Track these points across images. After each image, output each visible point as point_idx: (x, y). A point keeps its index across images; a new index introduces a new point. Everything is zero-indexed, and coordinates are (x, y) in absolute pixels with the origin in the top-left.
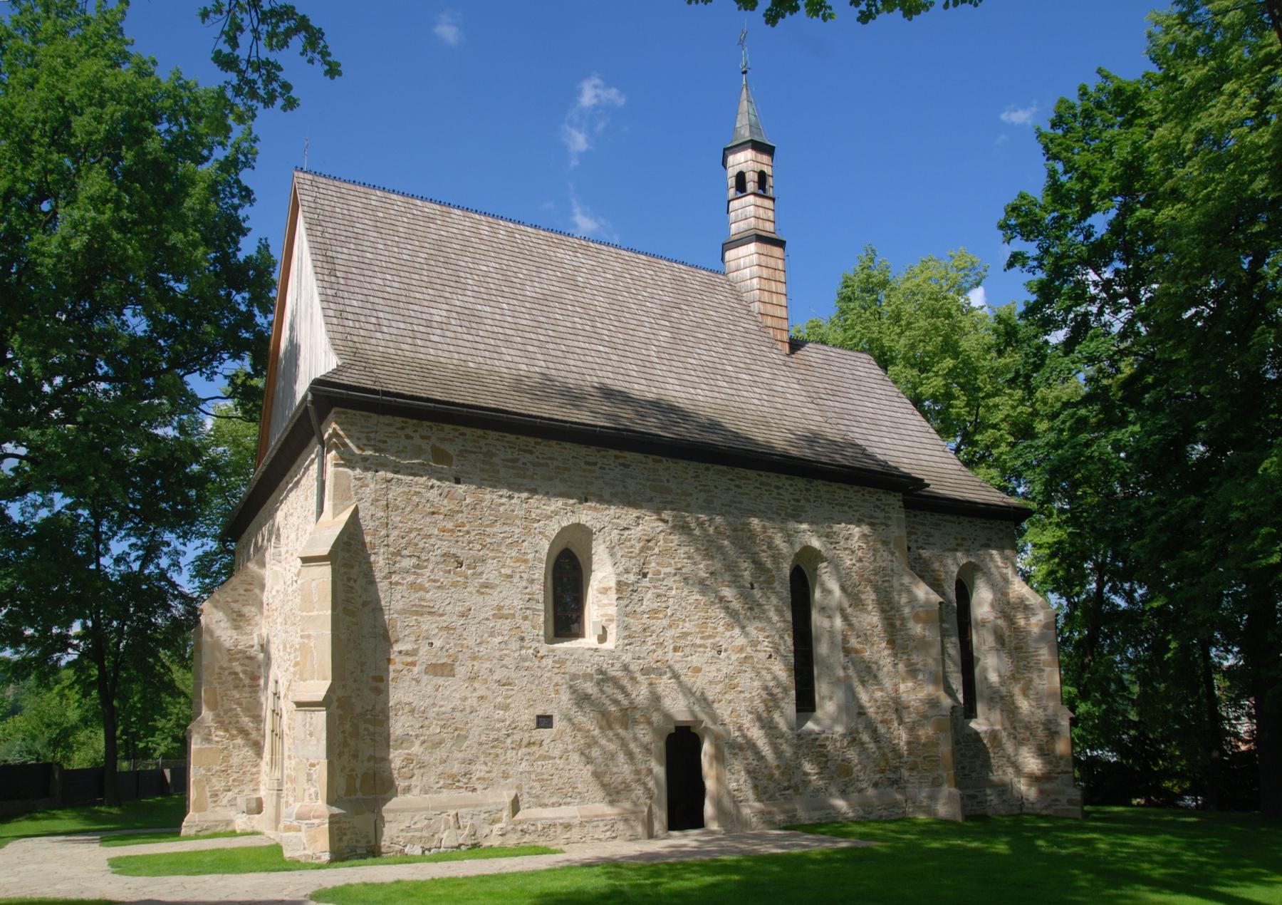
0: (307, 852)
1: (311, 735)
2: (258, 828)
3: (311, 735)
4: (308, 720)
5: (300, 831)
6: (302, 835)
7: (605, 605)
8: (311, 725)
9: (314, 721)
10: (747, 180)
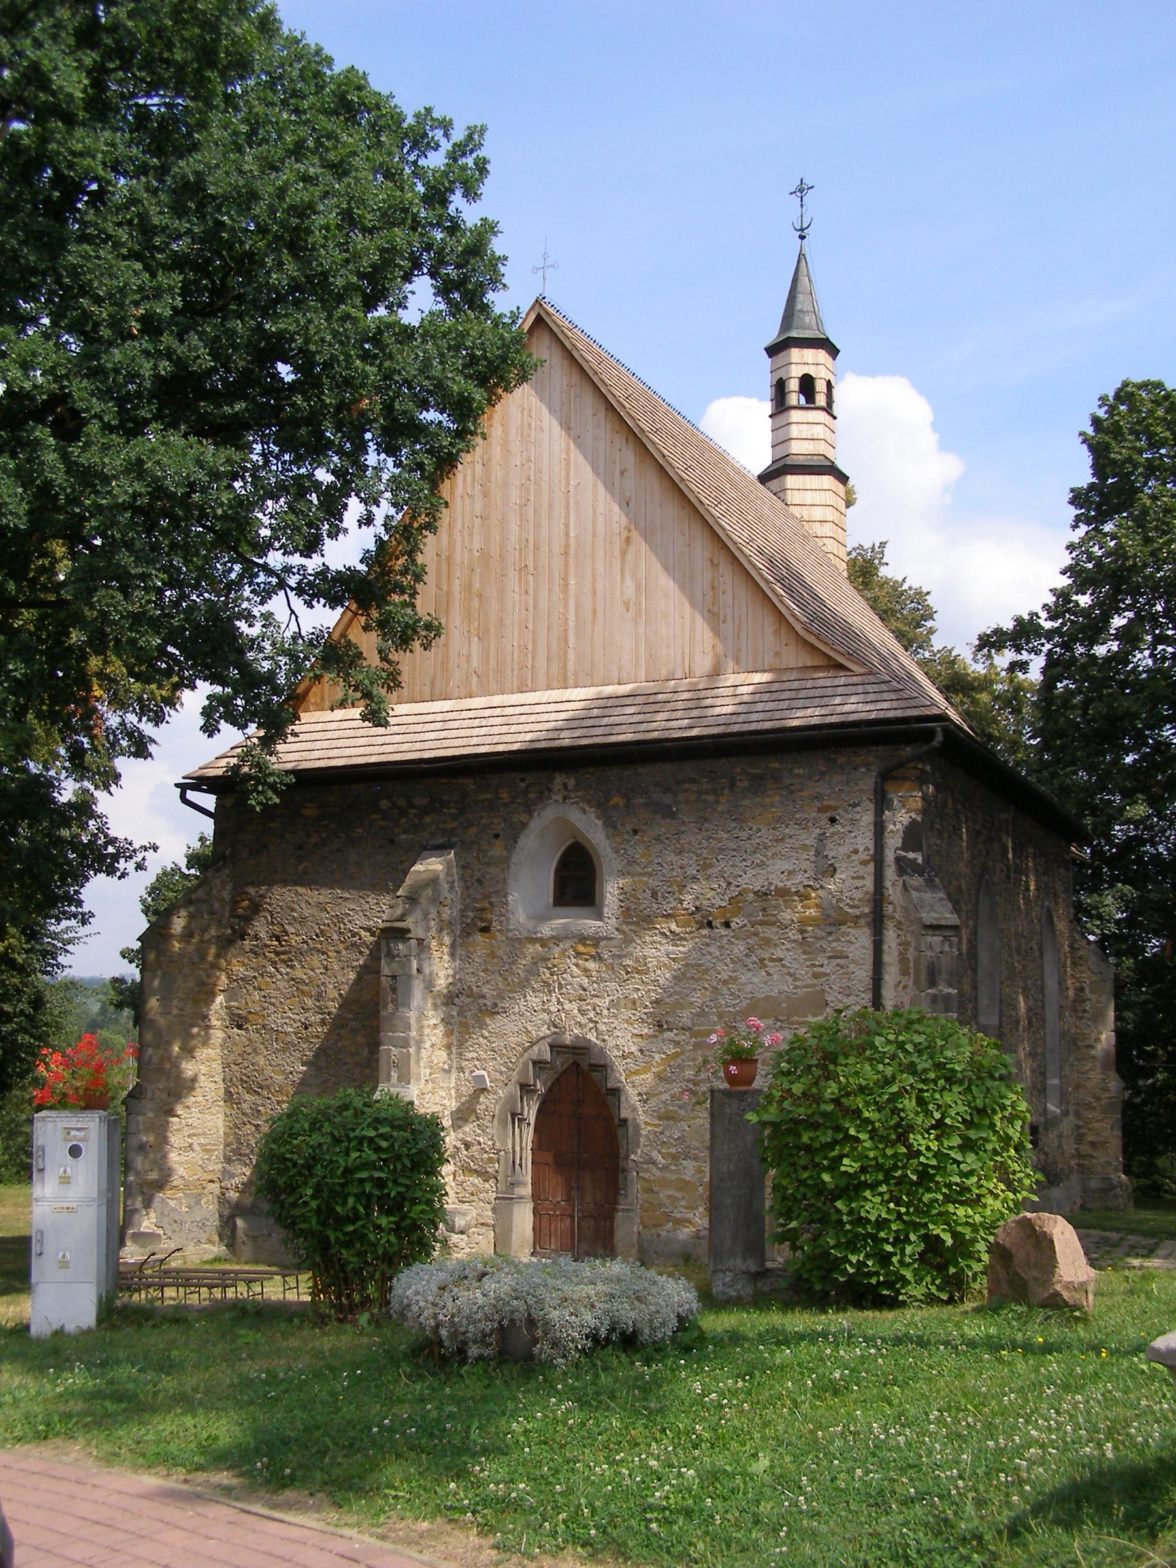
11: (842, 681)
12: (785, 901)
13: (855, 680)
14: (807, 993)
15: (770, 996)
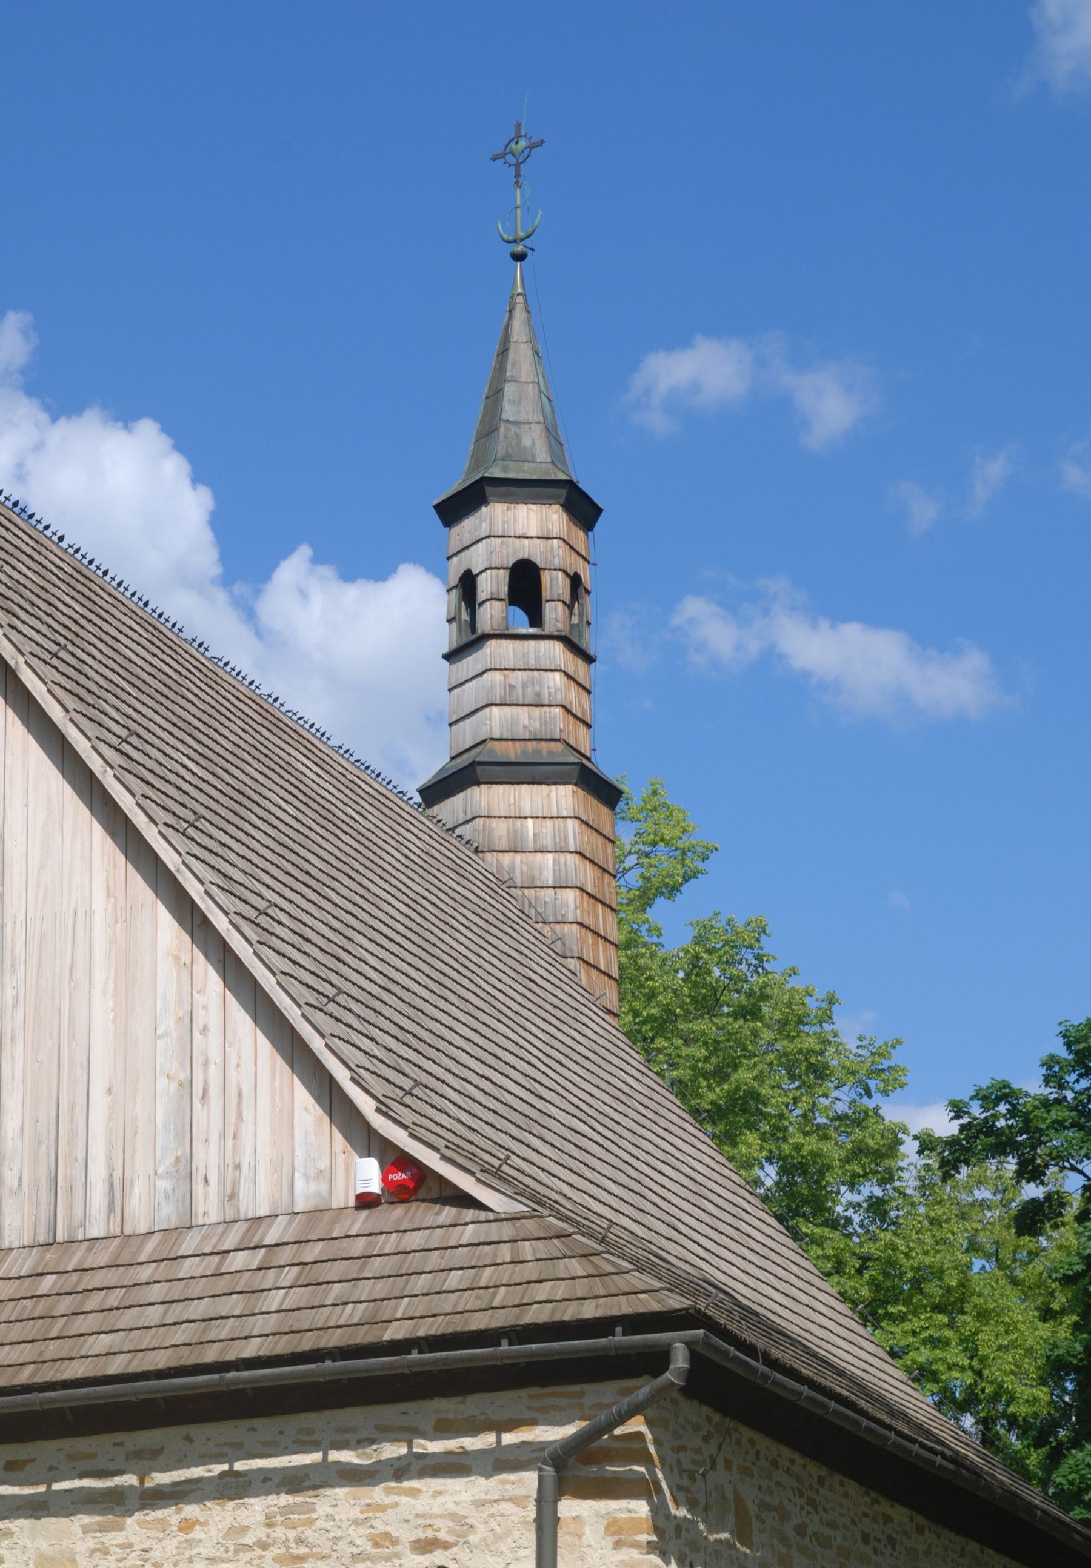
10: (546, 594)
11: (469, 1233)
13: (493, 1232)
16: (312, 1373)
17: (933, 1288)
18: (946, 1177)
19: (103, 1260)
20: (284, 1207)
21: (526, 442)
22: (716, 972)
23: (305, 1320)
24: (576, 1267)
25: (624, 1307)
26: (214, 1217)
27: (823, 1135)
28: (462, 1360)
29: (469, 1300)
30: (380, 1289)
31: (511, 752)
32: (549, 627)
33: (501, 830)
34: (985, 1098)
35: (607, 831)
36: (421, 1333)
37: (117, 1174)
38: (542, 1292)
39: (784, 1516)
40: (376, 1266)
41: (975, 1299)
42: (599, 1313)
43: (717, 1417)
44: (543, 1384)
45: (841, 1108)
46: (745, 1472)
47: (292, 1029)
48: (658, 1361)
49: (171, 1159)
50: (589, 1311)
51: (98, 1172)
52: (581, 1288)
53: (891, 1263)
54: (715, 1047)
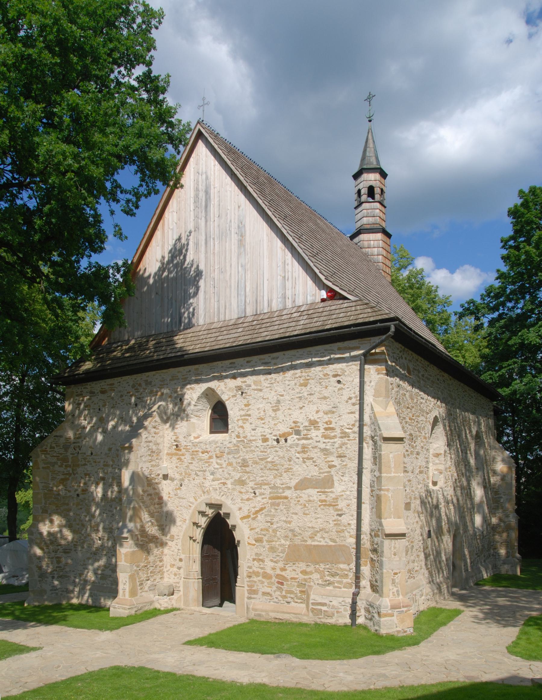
0: (398, 629)
1: (395, 554)
2: (175, 605)
3: (395, 554)
4: (393, 545)
5: (393, 616)
6: (394, 618)
7: (437, 464)
8: (395, 548)
9: (397, 546)
10: (376, 192)
11: (345, 305)
12: (315, 427)
13: (351, 304)
14: (325, 476)
15: (307, 478)
16: (309, 337)
17: (457, 345)
18: (460, 320)
19: (267, 317)
20: (305, 303)
21: (372, 160)
22: (413, 280)
23: (308, 326)
24: (369, 310)
25: (380, 318)
26: (290, 306)
27: (435, 315)
28: (342, 332)
29: (345, 319)
30: (325, 318)
31: (368, 227)
32: (376, 200)
33: (366, 244)
34: (468, 303)
35: (388, 243)
36: (333, 327)
37: (270, 298)
38: (361, 316)
39: (419, 372)
40: (325, 313)
41: (465, 348)
42: (374, 319)
43: (403, 347)
44: (362, 338)
45: (439, 310)
46: (410, 361)
47: (307, 262)
48: (388, 329)
49: (281, 294)
50: (372, 319)
51: (266, 298)
52: (370, 315)
53: (448, 341)
54: (413, 295)
